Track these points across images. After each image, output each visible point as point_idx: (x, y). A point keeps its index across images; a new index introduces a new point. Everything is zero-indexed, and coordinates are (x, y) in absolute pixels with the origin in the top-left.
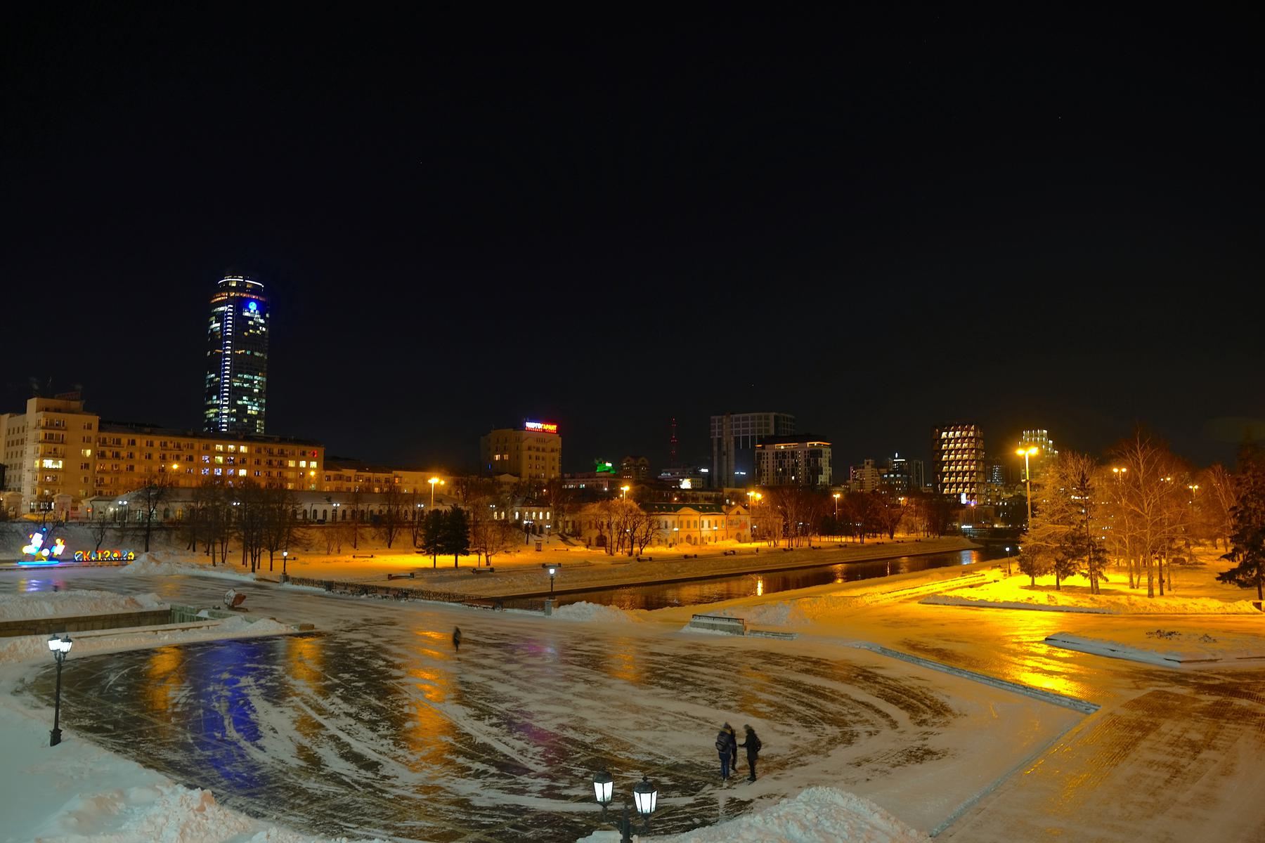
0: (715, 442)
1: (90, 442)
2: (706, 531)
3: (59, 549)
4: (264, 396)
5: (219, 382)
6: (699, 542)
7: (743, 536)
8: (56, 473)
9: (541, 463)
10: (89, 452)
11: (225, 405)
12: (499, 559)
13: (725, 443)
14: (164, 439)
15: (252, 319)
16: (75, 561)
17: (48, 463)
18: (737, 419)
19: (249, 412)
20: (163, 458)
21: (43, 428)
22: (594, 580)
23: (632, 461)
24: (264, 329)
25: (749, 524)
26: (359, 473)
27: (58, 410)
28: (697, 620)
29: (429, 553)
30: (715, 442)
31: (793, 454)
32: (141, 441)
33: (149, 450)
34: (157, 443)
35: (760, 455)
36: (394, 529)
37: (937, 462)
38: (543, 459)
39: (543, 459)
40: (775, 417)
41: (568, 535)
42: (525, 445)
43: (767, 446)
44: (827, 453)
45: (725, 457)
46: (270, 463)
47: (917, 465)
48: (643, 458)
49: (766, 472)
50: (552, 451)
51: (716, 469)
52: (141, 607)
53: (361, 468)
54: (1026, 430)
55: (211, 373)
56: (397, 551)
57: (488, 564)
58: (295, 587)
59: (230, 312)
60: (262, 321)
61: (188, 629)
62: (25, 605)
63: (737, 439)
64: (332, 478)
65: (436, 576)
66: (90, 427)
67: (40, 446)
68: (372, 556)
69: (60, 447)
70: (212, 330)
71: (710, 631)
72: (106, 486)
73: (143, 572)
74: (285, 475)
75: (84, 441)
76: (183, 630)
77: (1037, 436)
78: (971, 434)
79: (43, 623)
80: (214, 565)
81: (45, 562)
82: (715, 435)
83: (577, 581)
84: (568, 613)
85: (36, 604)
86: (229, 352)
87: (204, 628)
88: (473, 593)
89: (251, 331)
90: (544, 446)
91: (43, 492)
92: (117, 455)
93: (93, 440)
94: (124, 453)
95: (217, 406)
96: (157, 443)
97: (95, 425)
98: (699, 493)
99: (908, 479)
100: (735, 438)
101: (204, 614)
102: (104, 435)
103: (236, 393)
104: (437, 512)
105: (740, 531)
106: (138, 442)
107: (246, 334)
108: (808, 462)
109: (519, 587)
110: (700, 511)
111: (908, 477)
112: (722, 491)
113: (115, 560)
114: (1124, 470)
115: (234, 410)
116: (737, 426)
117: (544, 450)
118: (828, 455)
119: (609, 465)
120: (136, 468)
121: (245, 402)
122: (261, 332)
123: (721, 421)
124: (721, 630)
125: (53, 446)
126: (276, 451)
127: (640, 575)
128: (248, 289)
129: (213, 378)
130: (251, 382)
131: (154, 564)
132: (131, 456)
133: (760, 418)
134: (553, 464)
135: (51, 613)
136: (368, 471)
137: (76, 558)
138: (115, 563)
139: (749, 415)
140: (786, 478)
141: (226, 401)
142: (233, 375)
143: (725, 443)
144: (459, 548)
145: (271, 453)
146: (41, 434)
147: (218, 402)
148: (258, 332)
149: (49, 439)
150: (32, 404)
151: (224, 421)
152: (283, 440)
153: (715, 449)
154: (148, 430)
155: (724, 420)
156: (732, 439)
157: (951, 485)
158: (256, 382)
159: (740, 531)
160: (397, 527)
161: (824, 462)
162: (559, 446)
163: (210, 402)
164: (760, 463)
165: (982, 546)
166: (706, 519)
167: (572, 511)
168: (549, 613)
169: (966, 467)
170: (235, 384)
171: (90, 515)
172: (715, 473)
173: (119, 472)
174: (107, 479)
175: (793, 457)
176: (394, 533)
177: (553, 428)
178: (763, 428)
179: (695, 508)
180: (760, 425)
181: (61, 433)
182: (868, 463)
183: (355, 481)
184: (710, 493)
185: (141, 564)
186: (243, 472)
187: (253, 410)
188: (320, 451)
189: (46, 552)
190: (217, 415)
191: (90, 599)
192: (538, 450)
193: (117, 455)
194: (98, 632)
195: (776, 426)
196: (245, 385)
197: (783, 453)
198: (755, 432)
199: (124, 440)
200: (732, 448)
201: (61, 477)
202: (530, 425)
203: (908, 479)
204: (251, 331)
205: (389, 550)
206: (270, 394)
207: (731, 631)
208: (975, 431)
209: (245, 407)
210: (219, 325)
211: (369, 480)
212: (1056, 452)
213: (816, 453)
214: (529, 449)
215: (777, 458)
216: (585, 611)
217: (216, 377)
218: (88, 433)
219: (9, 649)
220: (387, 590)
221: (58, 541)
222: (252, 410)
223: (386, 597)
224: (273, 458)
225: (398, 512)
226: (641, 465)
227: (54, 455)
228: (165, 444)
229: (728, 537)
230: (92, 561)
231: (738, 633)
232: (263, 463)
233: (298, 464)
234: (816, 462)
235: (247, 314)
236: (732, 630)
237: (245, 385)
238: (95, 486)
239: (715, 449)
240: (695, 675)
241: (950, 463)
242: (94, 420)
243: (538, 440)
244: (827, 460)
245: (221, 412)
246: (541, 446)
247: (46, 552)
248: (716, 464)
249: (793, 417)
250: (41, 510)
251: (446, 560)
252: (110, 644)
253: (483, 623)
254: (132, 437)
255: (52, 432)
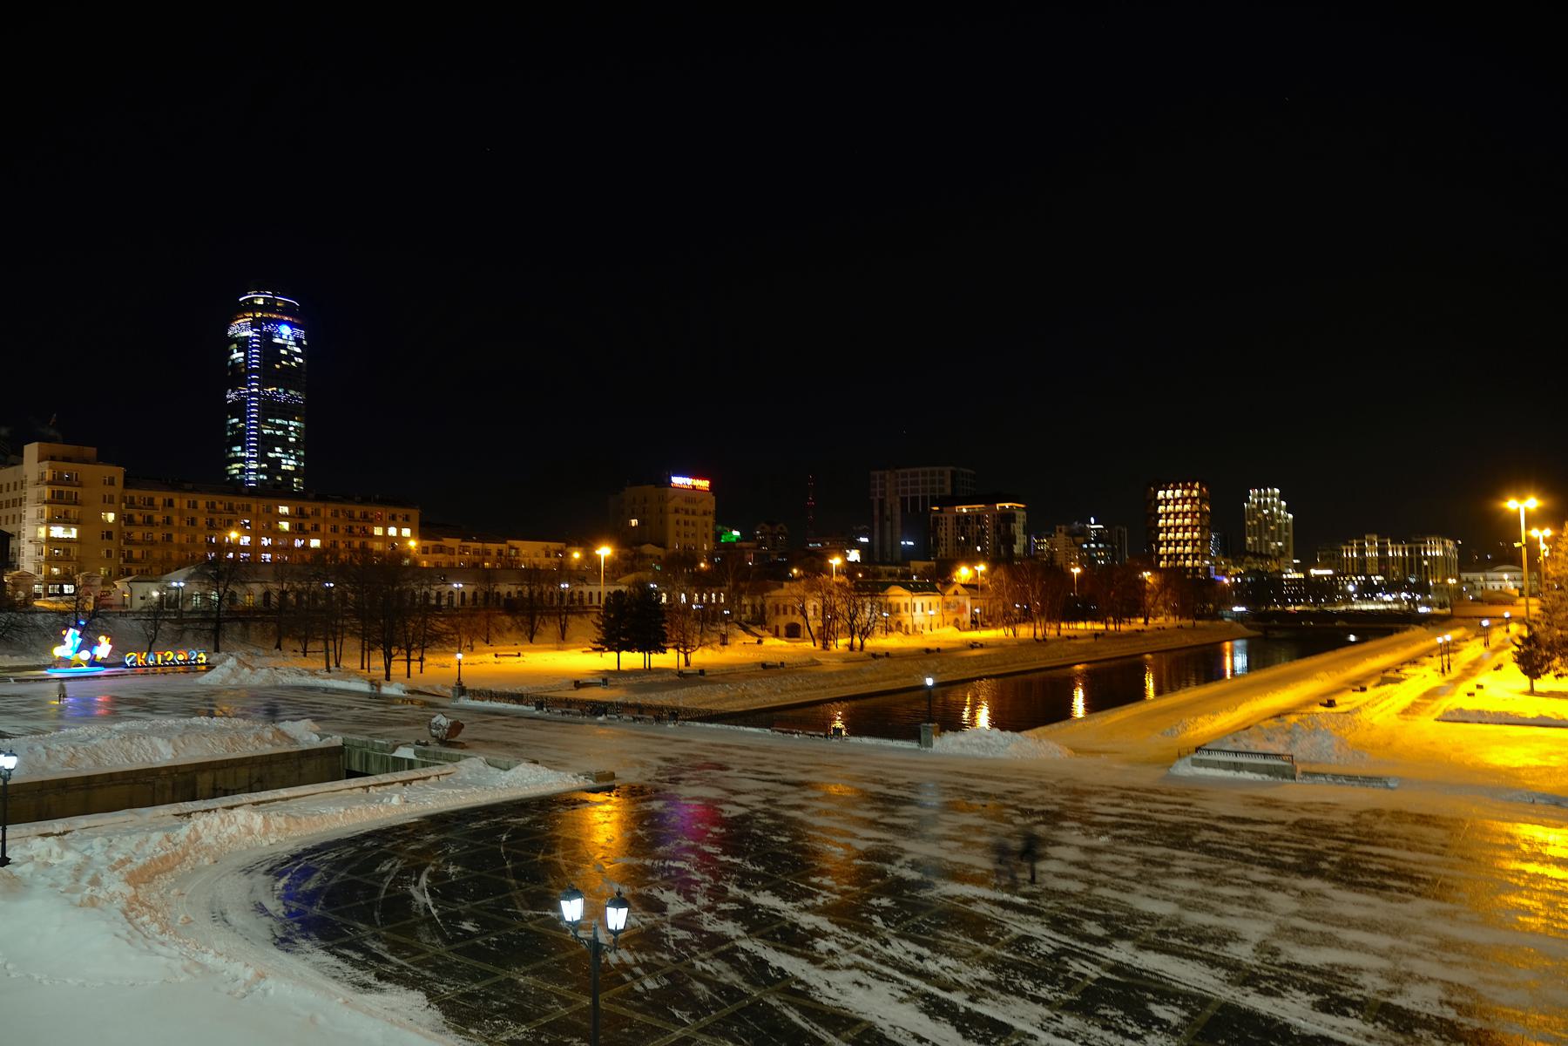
0: (876, 504)
1: (113, 503)
2: (919, 617)
3: (104, 649)
4: (302, 446)
5: (243, 428)
6: (910, 631)
7: (961, 621)
8: (67, 545)
9: (692, 530)
10: (111, 517)
11: (252, 459)
12: (703, 657)
13: (888, 505)
14: (211, 498)
15: (284, 347)
16: (127, 667)
17: (58, 532)
18: (904, 475)
19: (283, 467)
20: (211, 525)
21: (49, 483)
22: (844, 685)
23: (768, 528)
24: (301, 361)
25: (968, 606)
26: (464, 544)
27: (67, 459)
28: (1205, 756)
29: (611, 650)
30: (876, 504)
31: (979, 518)
32: (181, 501)
33: (192, 513)
34: (202, 504)
35: (936, 520)
36: (538, 617)
37: (1153, 528)
38: (693, 524)
39: (693, 524)
40: (952, 472)
41: (747, 622)
42: (671, 505)
43: (945, 509)
44: (1021, 517)
45: (888, 524)
46: (350, 530)
47: (1119, 532)
48: (781, 525)
49: (944, 542)
50: (705, 514)
51: (876, 537)
52: (294, 741)
53: (466, 537)
54: (1253, 488)
55: (232, 418)
56: (541, 646)
57: (687, 663)
58: (477, 703)
59: (256, 338)
60: (298, 350)
61: (410, 781)
62: (128, 743)
63: (904, 500)
64: (430, 550)
65: (635, 682)
66: (112, 482)
67: (45, 508)
68: (519, 655)
69: (74, 511)
70: (233, 360)
71: (1230, 774)
72: (136, 561)
73: (233, 682)
74: (370, 546)
75: (105, 501)
76: (404, 783)
77: (1266, 496)
78: (1195, 493)
79: (164, 772)
80: (329, 671)
81: (85, 668)
82: (876, 495)
83: (824, 687)
84: (962, 744)
85: (144, 742)
86: (256, 390)
87: (433, 779)
88: (703, 707)
89: (284, 362)
90: (695, 507)
91: (50, 572)
92: (149, 521)
93: (117, 500)
94: (158, 518)
95: (242, 460)
96: (202, 504)
97: (119, 480)
98: (881, 567)
99: (1113, 550)
100: (902, 499)
101: (406, 753)
102: (135, 493)
103: (266, 443)
104: (618, 594)
105: (958, 616)
106: (176, 501)
107: (278, 366)
108: (998, 529)
109: (757, 696)
110: (912, 590)
111: (1113, 548)
112: (909, 565)
113: (181, 665)
114: (903, 543)
115: (264, 465)
116: (916, 483)
117: (694, 513)
118: (1022, 520)
119: (736, 533)
120: (175, 537)
121: (278, 455)
122: (297, 363)
123: (883, 477)
124: (1251, 771)
125: (63, 508)
126: (357, 514)
127: (896, 678)
128: (279, 307)
129: (235, 424)
130: (284, 428)
131: (247, 670)
132: (168, 521)
133: (933, 473)
134: (706, 530)
135: (169, 757)
136: (476, 541)
137: (128, 662)
138: (180, 669)
139: (920, 470)
140: (970, 549)
141: (253, 453)
142: (263, 419)
143: (888, 505)
144: (653, 644)
145: (351, 517)
146: (47, 492)
147: (243, 454)
148: (293, 364)
149: (56, 499)
150: (31, 450)
151: (251, 478)
152: (365, 500)
153: (876, 512)
154: (190, 486)
155: (888, 476)
156: (898, 500)
157: (1186, 558)
158: (291, 429)
159: (958, 616)
160: (542, 615)
161: (1018, 528)
162: (712, 508)
163: (233, 455)
164: (935, 531)
165: (1259, 633)
166: (919, 600)
167: (753, 593)
168: (929, 744)
169: (1188, 535)
170: (265, 432)
171: (127, 602)
172: (876, 543)
173: (153, 543)
174: (137, 553)
175: (978, 522)
176: (537, 622)
177: (704, 484)
178: (937, 486)
179: (906, 586)
180: (933, 482)
181: (74, 490)
182: (1060, 531)
183: (460, 553)
184: (894, 568)
185: (230, 671)
186: (315, 543)
187: (289, 464)
188: (415, 514)
189: (85, 655)
190: (242, 471)
191: (221, 731)
192: (687, 512)
193: (149, 521)
194: (284, 793)
195: (953, 485)
196: (278, 433)
197: (966, 516)
198: (935, 492)
199: (159, 501)
200: (898, 511)
201: (75, 550)
202: (677, 481)
203: (1113, 548)
204: (284, 362)
205: (532, 646)
206: (310, 444)
207: (1270, 774)
208: (1200, 490)
209: (279, 459)
210: (242, 354)
211: (476, 552)
212: (1290, 516)
213: (1008, 517)
214: (677, 511)
215: (958, 523)
216: (990, 741)
217: (240, 422)
218: (108, 490)
219: (188, 837)
220: (569, 703)
221: (102, 639)
222: (287, 464)
223: (639, 720)
224: (354, 524)
225: (541, 594)
226: (779, 534)
227: (66, 521)
228: (213, 505)
229: (945, 624)
230: (149, 666)
231: (1284, 776)
232: (342, 531)
233: (385, 531)
234: (1008, 528)
235: (277, 340)
236: (1270, 771)
237: (278, 433)
238: (121, 562)
239: (876, 512)
240: (294, 712)
241: (1168, 529)
242: (118, 473)
243: (688, 500)
244: (1022, 525)
245: (246, 465)
246: (690, 507)
247: (85, 655)
248: (877, 530)
249: (973, 472)
250: (50, 595)
251: (632, 660)
252: (337, 819)
253: (1155, 801)
254: (168, 495)
255: (61, 488)
